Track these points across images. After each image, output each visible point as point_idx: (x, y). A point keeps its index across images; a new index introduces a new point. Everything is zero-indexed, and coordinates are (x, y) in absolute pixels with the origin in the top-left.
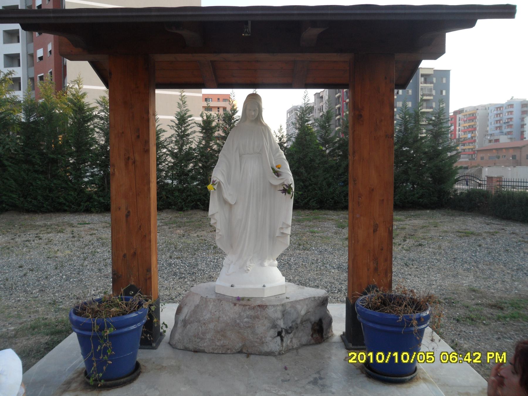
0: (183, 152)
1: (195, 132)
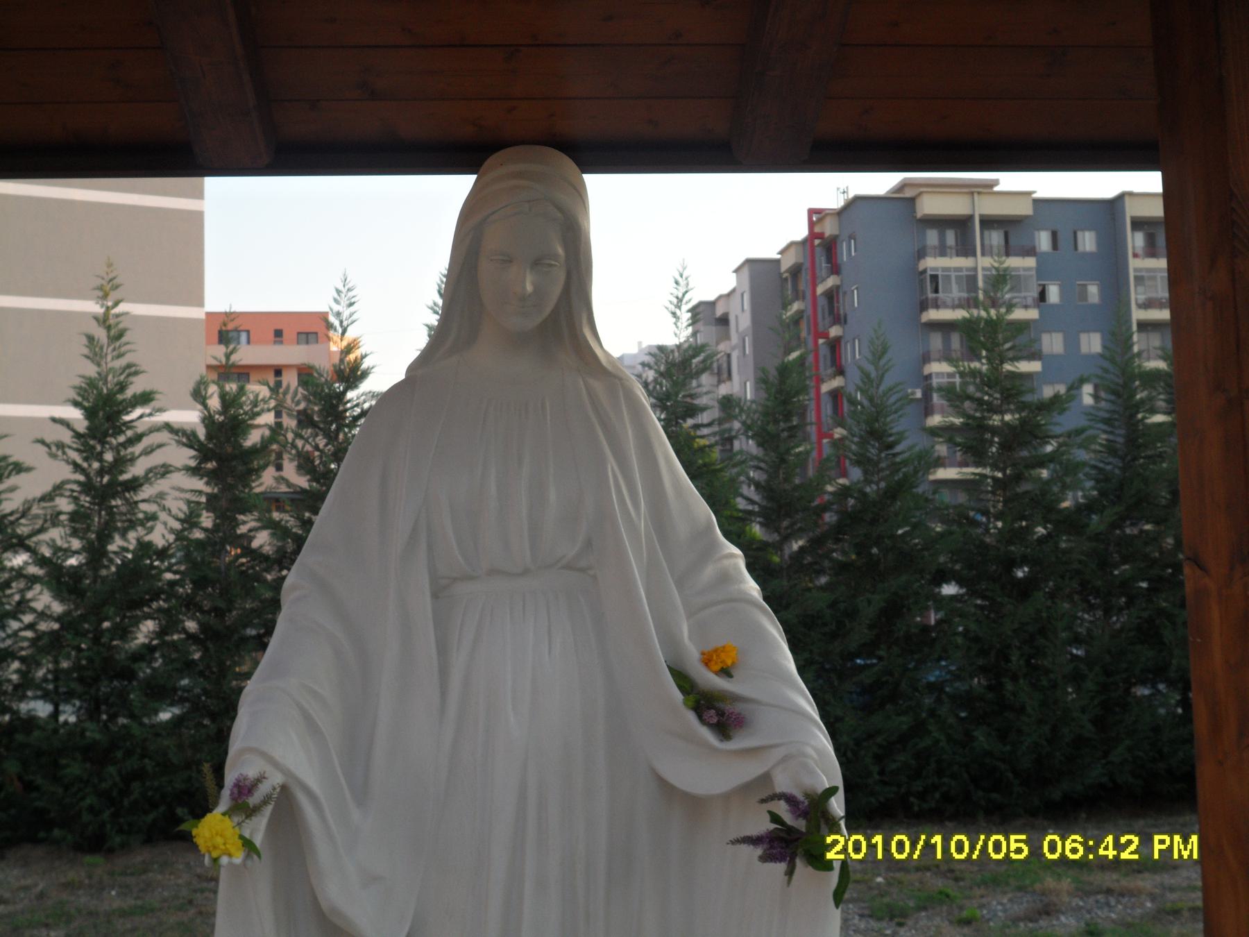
0: (107, 567)
1: (165, 470)
